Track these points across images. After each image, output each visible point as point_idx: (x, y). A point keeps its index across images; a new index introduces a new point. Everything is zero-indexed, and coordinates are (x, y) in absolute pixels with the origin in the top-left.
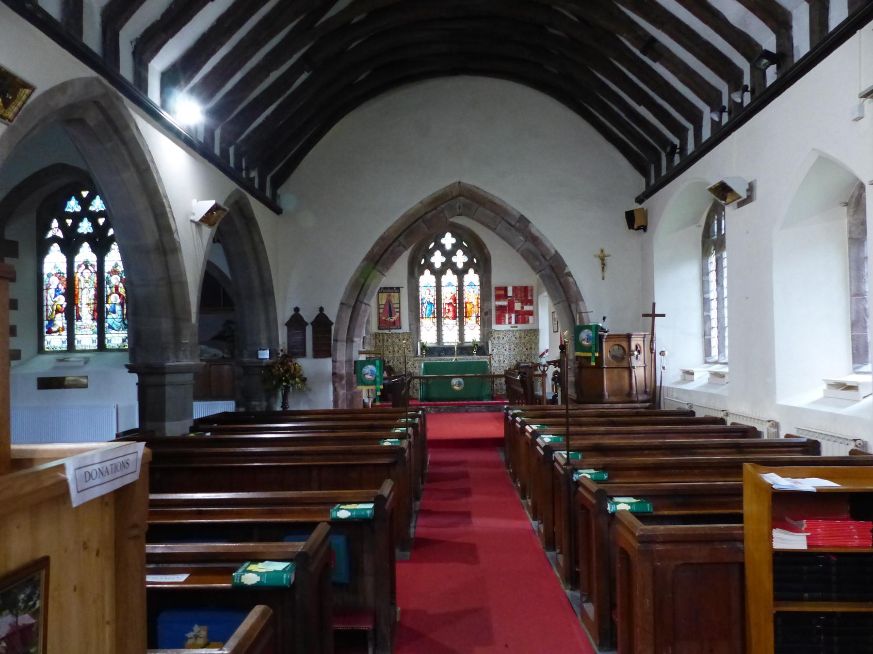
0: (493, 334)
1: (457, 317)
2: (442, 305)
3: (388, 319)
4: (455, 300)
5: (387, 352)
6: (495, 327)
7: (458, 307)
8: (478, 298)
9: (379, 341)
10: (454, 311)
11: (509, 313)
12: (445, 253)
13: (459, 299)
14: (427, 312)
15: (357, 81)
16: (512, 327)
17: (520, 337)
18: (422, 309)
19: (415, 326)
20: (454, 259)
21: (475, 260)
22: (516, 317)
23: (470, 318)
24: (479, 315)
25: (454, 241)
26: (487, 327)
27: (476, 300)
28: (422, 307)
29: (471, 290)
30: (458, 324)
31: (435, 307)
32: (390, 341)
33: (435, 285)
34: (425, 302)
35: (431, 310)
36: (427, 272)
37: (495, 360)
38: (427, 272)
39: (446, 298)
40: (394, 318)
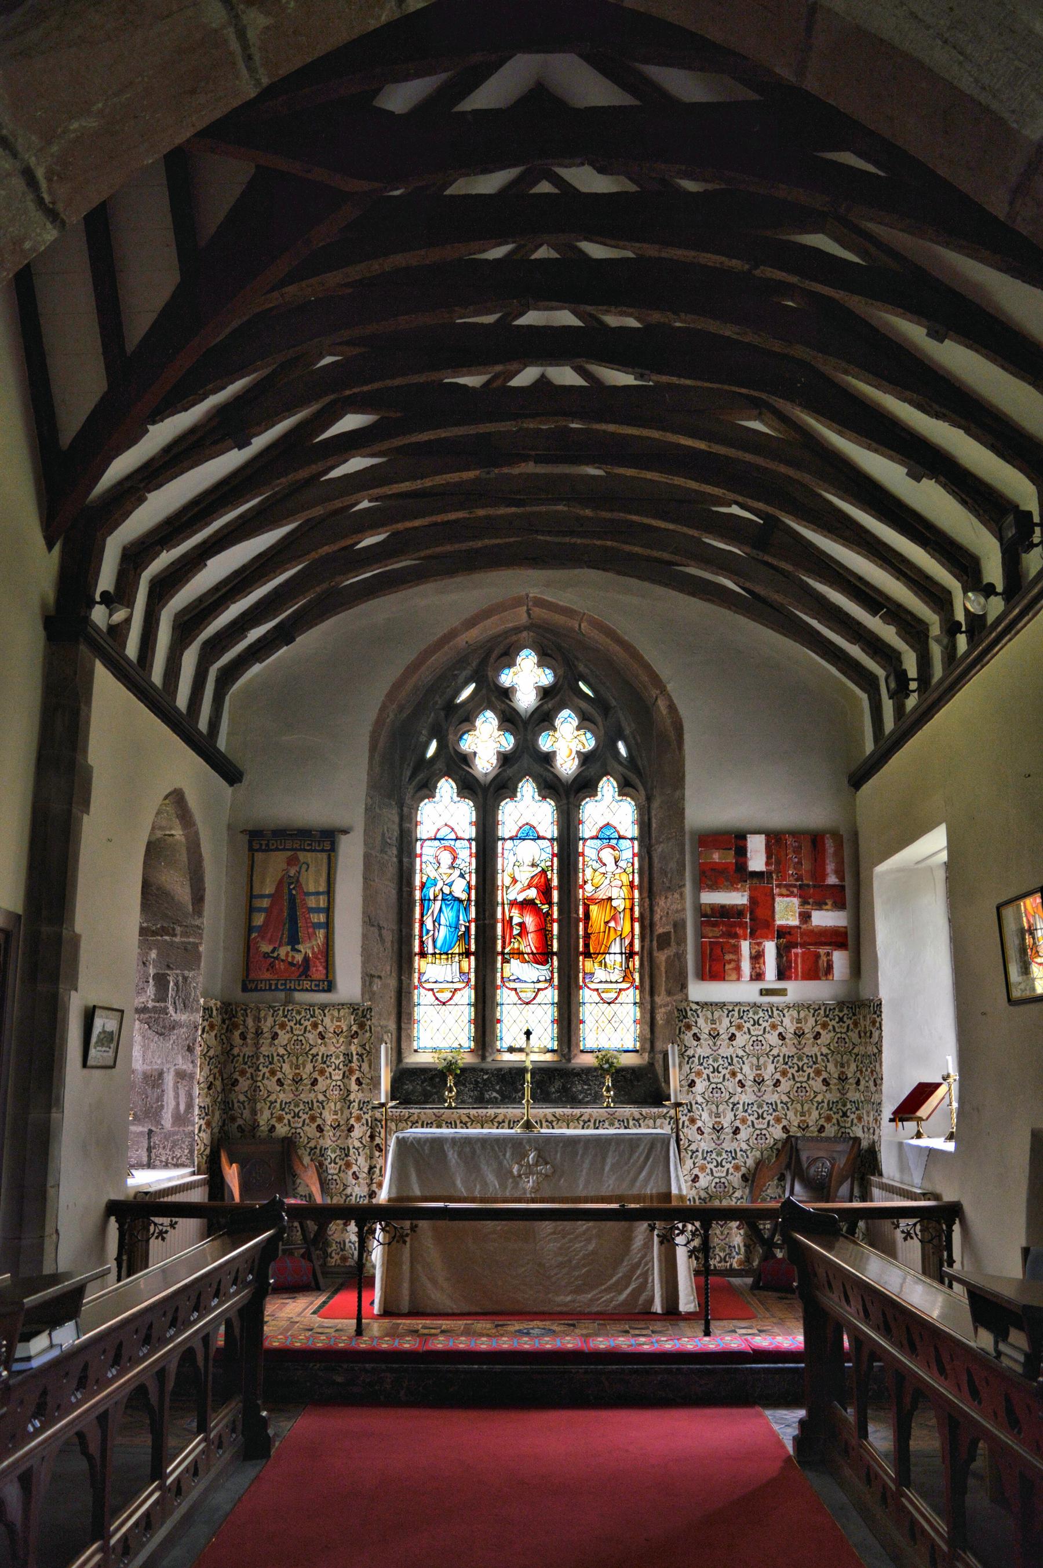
0: (691, 1020)
1: (553, 954)
2: (499, 909)
3: (283, 951)
4: (545, 891)
5: (271, 1084)
6: (699, 991)
7: (555, 916)
8: (632, 883)
9: (243, 1036)
10: (543, 933)
11: (753, 935)
12: (510, 719)
13: (560, 888)
14: (443, 933)
15: (359, 546)
16: (764, 992)
17: (799, 1034)
18: (422, 923)
19: (393, 983)
20: (545, 743)
21: (621, 747)
22: (782, 953)
23: (600, 958)
24: (637, 948)
25: (546, 678)
26: (669, 993)
27: (624, 892)
28: (422, 915)
29: (607, 855)
30: (556, 982)
31: (473, 915)
32: (283, 1037)
33: (474, 836)
34: (435, 897)
35: (457, 927)
36: (446, 787)
37: (699, 1124)
38: (446, 787)
39: (515, 881)
40: (307, 948)
